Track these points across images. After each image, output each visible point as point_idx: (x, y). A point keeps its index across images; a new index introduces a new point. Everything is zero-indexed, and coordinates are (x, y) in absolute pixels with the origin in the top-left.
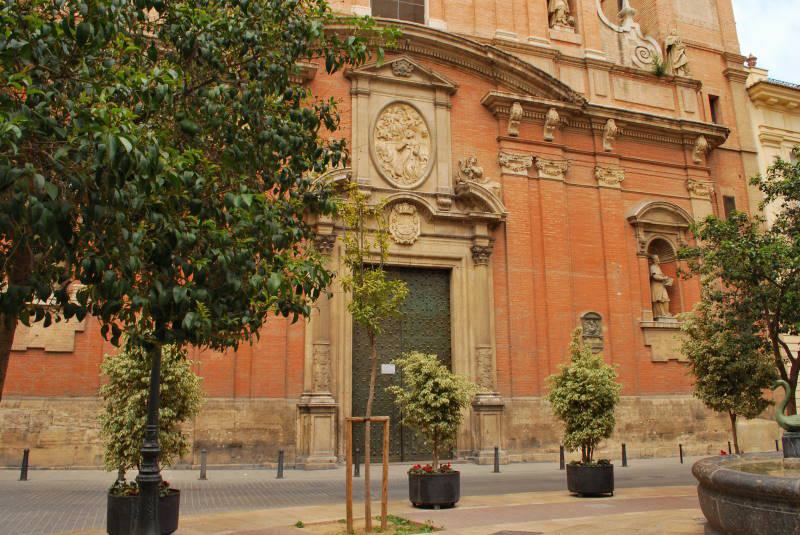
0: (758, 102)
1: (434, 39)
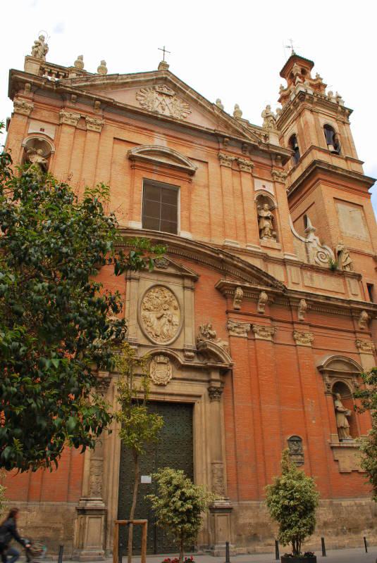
1: (184, 244)
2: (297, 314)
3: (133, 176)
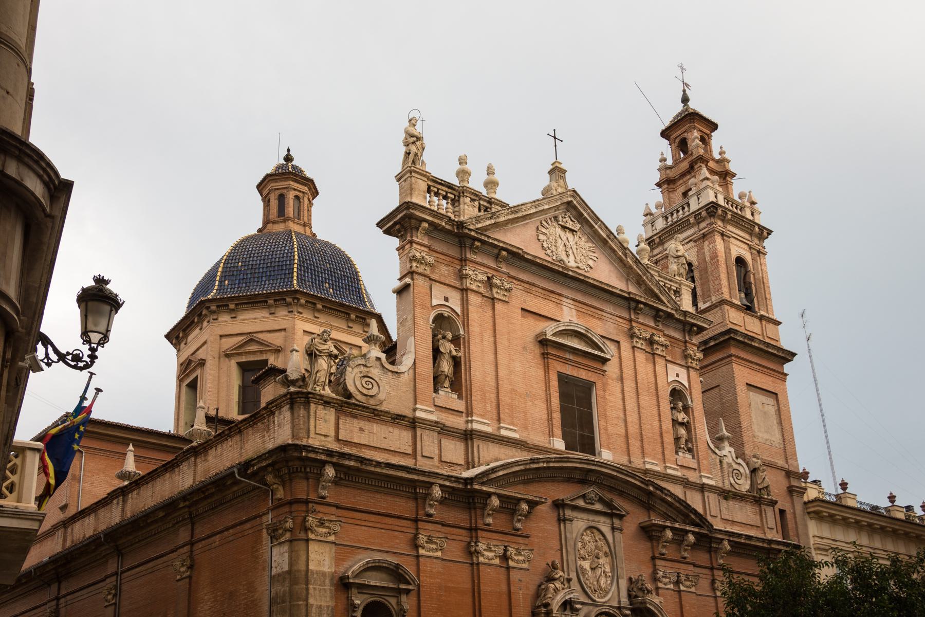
0: (812, 515)
1: (615, 474)
2: (424, 505)
3: (546, 368)
